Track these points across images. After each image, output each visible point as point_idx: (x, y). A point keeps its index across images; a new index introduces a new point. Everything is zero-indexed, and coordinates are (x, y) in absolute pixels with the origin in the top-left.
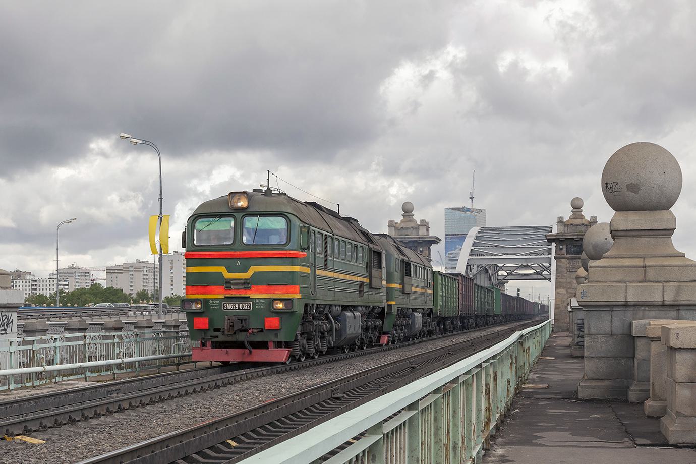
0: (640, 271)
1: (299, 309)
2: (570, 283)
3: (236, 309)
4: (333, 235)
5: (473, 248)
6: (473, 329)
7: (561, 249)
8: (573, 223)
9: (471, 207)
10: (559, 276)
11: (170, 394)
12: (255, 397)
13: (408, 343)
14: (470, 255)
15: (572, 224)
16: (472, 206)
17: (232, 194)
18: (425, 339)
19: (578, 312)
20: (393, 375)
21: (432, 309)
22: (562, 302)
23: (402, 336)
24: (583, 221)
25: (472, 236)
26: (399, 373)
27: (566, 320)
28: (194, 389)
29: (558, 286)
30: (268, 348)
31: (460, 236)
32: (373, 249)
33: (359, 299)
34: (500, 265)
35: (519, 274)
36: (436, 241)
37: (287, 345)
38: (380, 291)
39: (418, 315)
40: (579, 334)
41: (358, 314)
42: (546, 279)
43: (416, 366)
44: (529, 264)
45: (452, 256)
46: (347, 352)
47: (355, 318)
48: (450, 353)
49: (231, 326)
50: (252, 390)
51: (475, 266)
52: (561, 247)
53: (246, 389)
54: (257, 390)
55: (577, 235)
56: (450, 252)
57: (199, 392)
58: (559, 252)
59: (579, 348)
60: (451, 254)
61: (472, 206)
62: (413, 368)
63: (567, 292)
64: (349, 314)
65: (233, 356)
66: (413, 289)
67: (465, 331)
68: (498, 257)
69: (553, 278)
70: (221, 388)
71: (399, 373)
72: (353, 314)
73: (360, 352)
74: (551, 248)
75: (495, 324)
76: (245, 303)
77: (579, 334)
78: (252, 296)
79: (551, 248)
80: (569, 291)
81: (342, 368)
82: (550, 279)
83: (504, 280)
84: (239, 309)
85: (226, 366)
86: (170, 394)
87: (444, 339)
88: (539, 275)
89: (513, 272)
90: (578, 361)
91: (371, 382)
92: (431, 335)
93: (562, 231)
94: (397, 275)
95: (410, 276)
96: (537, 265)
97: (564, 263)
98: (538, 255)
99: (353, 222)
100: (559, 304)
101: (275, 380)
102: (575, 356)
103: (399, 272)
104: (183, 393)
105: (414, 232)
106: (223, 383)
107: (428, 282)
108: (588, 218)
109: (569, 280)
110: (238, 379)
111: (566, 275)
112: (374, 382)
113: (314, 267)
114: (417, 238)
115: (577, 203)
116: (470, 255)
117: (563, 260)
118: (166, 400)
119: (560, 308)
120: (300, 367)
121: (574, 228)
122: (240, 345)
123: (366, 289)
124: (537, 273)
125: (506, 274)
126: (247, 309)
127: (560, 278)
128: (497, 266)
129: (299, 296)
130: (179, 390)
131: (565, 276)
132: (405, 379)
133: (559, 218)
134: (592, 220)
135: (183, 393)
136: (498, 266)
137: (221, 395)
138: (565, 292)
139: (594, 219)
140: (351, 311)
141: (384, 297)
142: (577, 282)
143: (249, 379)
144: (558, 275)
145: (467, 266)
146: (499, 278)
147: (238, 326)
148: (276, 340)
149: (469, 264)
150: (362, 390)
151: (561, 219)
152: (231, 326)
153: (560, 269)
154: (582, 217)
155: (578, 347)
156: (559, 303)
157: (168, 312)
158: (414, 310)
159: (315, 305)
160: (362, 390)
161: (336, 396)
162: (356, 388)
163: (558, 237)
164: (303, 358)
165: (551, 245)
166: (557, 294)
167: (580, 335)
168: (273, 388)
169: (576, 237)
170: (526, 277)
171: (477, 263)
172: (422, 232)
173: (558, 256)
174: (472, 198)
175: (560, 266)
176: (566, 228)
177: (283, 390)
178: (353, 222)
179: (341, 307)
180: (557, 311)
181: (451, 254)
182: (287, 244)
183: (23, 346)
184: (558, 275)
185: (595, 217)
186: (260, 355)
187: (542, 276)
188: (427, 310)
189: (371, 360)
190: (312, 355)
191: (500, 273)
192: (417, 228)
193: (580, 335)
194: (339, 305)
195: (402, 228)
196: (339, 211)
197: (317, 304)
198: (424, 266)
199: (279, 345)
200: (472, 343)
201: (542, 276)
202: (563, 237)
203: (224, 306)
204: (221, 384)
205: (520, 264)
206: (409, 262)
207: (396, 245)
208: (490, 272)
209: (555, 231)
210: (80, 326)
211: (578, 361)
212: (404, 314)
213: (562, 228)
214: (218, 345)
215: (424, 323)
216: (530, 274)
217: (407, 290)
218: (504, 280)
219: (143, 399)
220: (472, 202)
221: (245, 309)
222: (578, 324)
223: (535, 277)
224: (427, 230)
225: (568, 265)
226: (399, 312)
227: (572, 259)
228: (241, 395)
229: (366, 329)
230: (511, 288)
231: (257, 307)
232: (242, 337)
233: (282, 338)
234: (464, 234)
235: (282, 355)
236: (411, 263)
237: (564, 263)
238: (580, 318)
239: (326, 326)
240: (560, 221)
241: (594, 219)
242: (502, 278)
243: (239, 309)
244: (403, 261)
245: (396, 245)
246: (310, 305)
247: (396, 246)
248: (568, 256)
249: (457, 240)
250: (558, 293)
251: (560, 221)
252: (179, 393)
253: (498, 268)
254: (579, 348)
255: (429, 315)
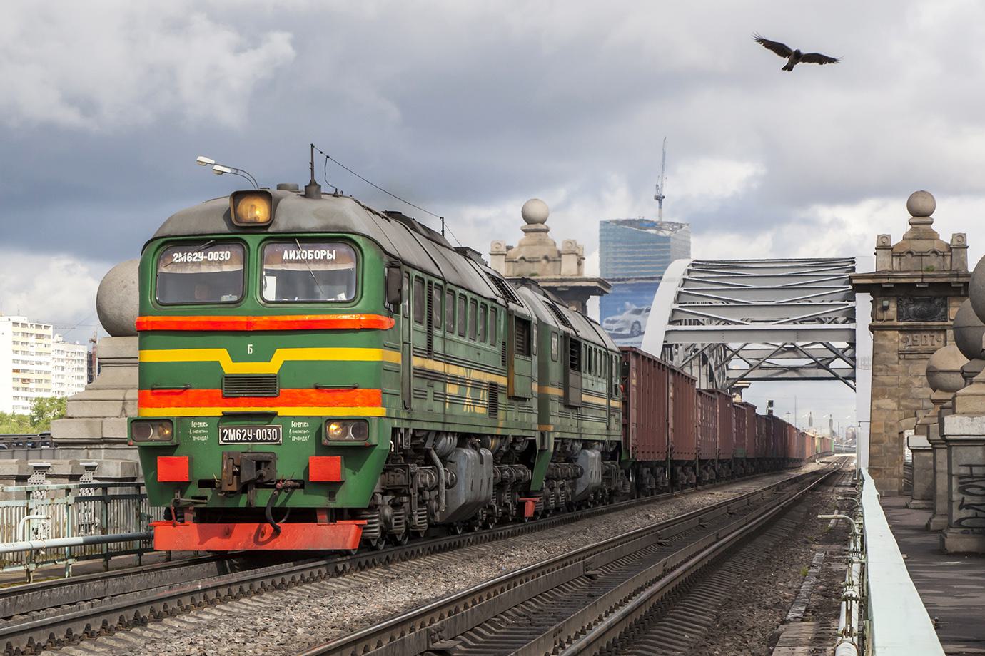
0: (867, 362)
1: (381, 440)
2: (907, 385)
3: (248, 441)
4: (445, 283)
5: (676, 306)
6: (665, 494)
7: (885, 309)
8: (912, 249)
9: (656, 219)
10: (881, 370)
11: (31, 640)
12: (235, 646)
13: (569, 515)
14: (671, 323)
15: (910, 252)
16: (660, 216)
17: (238, 196)
18: (602, 508)
19: (961, 450)
20: (551, 594)
21: (620, 441)
22: (888, 429)
23: (420, 520)
24: (936, 246)
25: (668, 280)
26: (564, 590)
27: (896, 470)
28: (88, 627)
29: (878, 391)
30: (316, 522)
31: (633, 282)
32: (515, 314)
33: (489, 422)
34: (734, 346)
35: (776, 367)
36: (600, 289)
37: (354, 514)
38: (527, 403)
39: (594, 454)
40: (963, 498)
41: (487, 453)
42: (837, 378)
43: (597, 572)
44: (799, 344)
45: (615, 326)
46: (459, 532)
47: (482, 463)
48: (660, 544)
49: (234, 473)
50: (223, 630)
51: (680, 348)
52: (886, 303)
53: (209, 627)
54: (237, 630)
55: (923, 277)
56: (610, 318)
57: (99, 634)
58: (880, 315)
59: (962, 533)
60: (614, 322)
61: (660, 216)
62: (590, 577)
63: (899, 405)
64: (469, 453)
65: (242, 537)
66: (585, 398)
67: (644, 498)
68: (733, 327)
69: (864, 376)
70: (149, 626)
71: (564, 590)
72: (479, 453)
73: (485, 533)
74: (853, 308)
75: (700, 484)
76: (266, 428)
77: (963, 498)
78: (282, 411)
79: (853, 308)
80: (903, 403)
81: (420, 577)
82: (854, 379)
83: (742, 378)
84: (254, 439)
85: (222, 560)
86: (31, 640)
87: (626, 511)
88: (821, 369)
89: (764, 361)
90: (965, 563)
91: (509, 612)
92: (615, 498)
93: (888, 267)
94: (555, 370)
95: (579, 370)
96: (821, 346)
97: (892, 340)
98: (823, 322)
99: (474, 256)
100: (881, 434)
101: (273, 606)
102: (953, 551)
103: (559, 361)
104: (62, 637)
105: (550, 267)
106: (152, 611)
107: (614, 383)
108: (946, 238)
109: (903, 380)
110: (212, 595)
111: (897, 366)
112: (515, 612)
113: (406, 349)
114: (555, 280)
115: (922, 204)
116: (671, 323)
117: (890, 334)
118: (22, 653)
119: (882, 442)
120: (287, 582)
121: (915, 260)
122: (253, 515)
123: (502, 399)
124: (819, 366)
125: (747, 366)
126: (241, 441)
127: (883, 373)
128: (726, 348)
129: (379, 411)
130: (51, 630)
131: (894, 370)
132: (596, 604)
133: (881, 237)
134: (955, 243)
135: (62, 637)
136: (729, 349)
137: (153, 642)
138: (894, 406)
139: (960, 239)
140: (474, 447)
141: (535, 418)
142: (929, 381)
143: (212, 603)
144: (879, 367)
145: (664, 346)
146: (730, 374)
147: (248, 474)
148: (332, 505)
149: (669, 343)
150: (491, 632)
151: (884, 240)
152: (234, 473)
153: (882, 354)
154: (933, 236)
155: (960, 530)
156: (882, 430)
157: (33, 447)
158: (587, 444)
159: (411, 432)
160: (491, 632)
161: (590, 572)
162: (479, 626)
163: (878, 281)
164: (381, 544)
165: (854, 300)
166: (875, 410)
167: (965, 503)
168: (273, 624)
169: (920, 280)
170: (794, 374)
171: (687, 341)
172: (568, 267)
173: (879, 323)
174: (659, 199)
175: (882, 346)
176: (896, 261)
177: (300, 631)
178: (474, 256)
179: (456, 439)
180: (875, 448)
181: (614, 322)
182: (358, 300)
183: (16, 499)
184: (879, 367)
185: (962, 236)
186: (297, 537)
187: (830, 370)
188: (611, 445)
189: (480, 558)
190: (374, 544)
191: (733, 364)
192: (556, 258)
193: (965, 503)
194: (453, 434)
195: (523, 258)
196: (443, 231)
197: (414, 430)
198: (607, 349)
199: (337, 515)
200: (701, 520)
201: (830, 370)
202: (890, 280)
203: (223, 435)
204: (147, 614)
205: (780, 344)
206: (578, 340)
207: (550, 303)
208: (712, 361)
209: (867, 265)
210: (19, 472)
211: (965, 563)
212: (566, 452)
213: (887, 259)
214: (206, 516)
215: (606, 474)
216: (802, 367)
217: (573, 400)
218: (742, 378)
219: (34, 635)
220: (660, 208)
221: (267, 440)
222: (961, 477)
223: (813, 373)
224: (579, 264)
225: (901, 346)
226: (558, 449)
227: (911, 330)
228: (201, 643)
229: (499, 486)
230: (757, 396)
231: (294, 438)
232: (262, 498)
233: (343, 500)
234: (652, 278)
235: (344, 535)
236: (583, 342)
237: (892, 340)
238: (964, 462)
239: (431, 476)
240: (883, 245)
241: (960, 239)
242: (737, 375)
243: (254, 439)
244: (566, 335)
245: (550, 303)
246: (402, 431)
247: (549, 305)
248: (902, 324)
249: (624, 290)
250: (878, 408)
251: (883, 245)
252: (52, 636)
253: (729, 353)
254: (962, 533)
255: (613, 456)
